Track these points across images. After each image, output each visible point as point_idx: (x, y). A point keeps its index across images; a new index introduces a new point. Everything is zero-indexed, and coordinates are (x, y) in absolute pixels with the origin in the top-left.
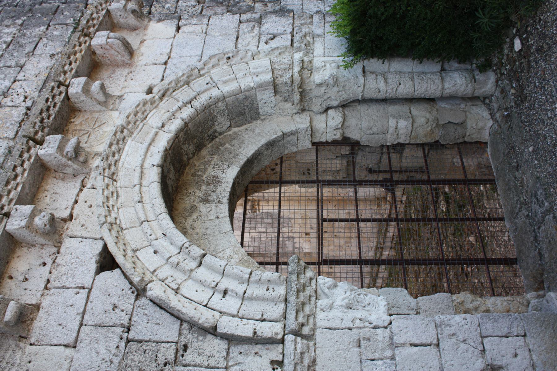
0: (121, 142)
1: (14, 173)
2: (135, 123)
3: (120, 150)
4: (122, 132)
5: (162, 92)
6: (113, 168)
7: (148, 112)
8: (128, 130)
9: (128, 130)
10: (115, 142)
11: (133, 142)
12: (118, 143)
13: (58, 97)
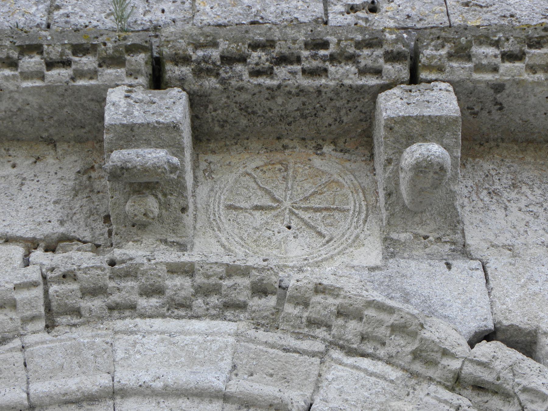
0: (214, 300)
1: (15, 55)
2: (312, 323)
3: (180, 306)
4: (260, 290)
5: (487, 376)
6: (96, 304)
7: (382, 352)
8: (278, 310)
9: (278, 310)
10: (199, 279)
11: (231, 340)
12: (204, 291)
13: (351, 68)
